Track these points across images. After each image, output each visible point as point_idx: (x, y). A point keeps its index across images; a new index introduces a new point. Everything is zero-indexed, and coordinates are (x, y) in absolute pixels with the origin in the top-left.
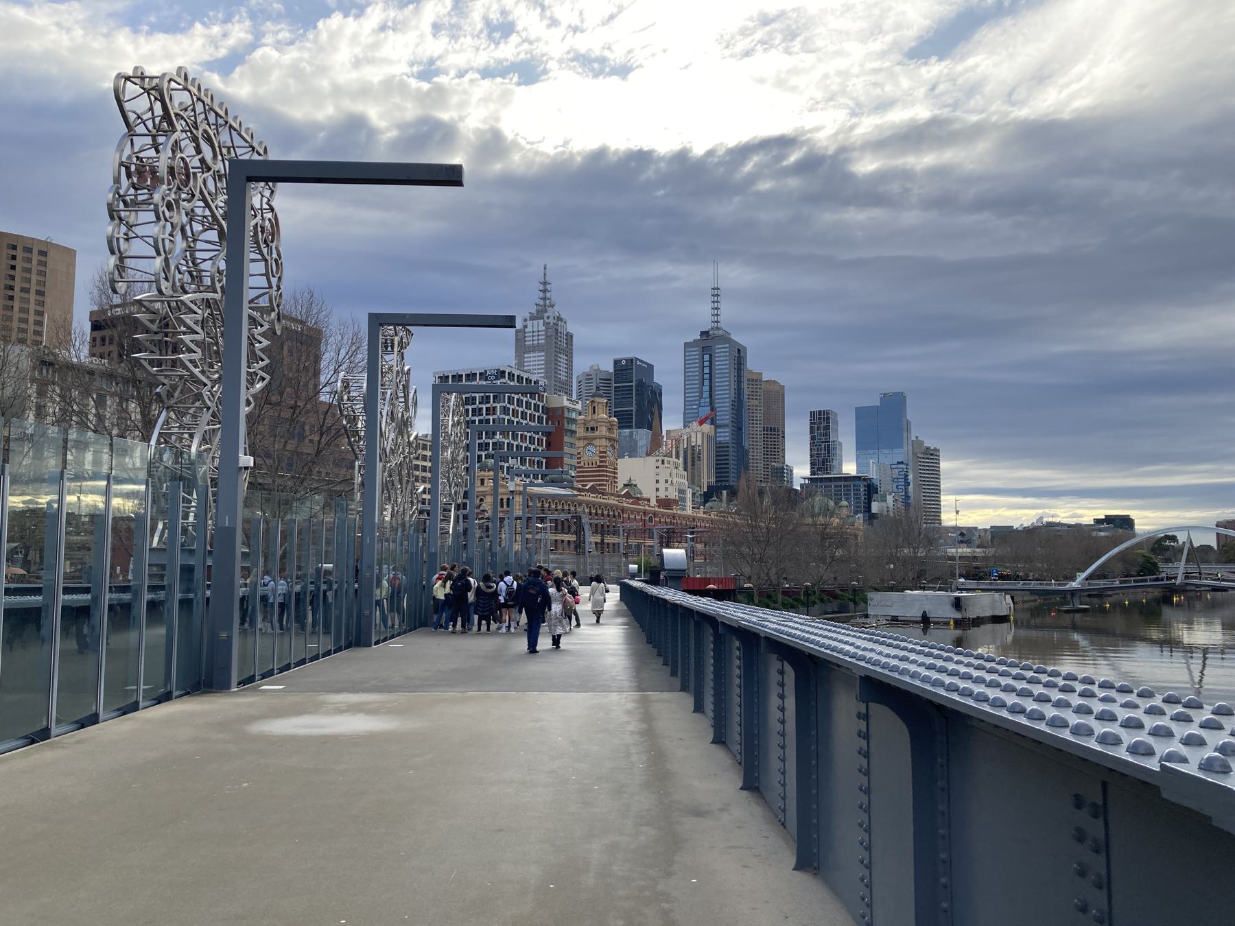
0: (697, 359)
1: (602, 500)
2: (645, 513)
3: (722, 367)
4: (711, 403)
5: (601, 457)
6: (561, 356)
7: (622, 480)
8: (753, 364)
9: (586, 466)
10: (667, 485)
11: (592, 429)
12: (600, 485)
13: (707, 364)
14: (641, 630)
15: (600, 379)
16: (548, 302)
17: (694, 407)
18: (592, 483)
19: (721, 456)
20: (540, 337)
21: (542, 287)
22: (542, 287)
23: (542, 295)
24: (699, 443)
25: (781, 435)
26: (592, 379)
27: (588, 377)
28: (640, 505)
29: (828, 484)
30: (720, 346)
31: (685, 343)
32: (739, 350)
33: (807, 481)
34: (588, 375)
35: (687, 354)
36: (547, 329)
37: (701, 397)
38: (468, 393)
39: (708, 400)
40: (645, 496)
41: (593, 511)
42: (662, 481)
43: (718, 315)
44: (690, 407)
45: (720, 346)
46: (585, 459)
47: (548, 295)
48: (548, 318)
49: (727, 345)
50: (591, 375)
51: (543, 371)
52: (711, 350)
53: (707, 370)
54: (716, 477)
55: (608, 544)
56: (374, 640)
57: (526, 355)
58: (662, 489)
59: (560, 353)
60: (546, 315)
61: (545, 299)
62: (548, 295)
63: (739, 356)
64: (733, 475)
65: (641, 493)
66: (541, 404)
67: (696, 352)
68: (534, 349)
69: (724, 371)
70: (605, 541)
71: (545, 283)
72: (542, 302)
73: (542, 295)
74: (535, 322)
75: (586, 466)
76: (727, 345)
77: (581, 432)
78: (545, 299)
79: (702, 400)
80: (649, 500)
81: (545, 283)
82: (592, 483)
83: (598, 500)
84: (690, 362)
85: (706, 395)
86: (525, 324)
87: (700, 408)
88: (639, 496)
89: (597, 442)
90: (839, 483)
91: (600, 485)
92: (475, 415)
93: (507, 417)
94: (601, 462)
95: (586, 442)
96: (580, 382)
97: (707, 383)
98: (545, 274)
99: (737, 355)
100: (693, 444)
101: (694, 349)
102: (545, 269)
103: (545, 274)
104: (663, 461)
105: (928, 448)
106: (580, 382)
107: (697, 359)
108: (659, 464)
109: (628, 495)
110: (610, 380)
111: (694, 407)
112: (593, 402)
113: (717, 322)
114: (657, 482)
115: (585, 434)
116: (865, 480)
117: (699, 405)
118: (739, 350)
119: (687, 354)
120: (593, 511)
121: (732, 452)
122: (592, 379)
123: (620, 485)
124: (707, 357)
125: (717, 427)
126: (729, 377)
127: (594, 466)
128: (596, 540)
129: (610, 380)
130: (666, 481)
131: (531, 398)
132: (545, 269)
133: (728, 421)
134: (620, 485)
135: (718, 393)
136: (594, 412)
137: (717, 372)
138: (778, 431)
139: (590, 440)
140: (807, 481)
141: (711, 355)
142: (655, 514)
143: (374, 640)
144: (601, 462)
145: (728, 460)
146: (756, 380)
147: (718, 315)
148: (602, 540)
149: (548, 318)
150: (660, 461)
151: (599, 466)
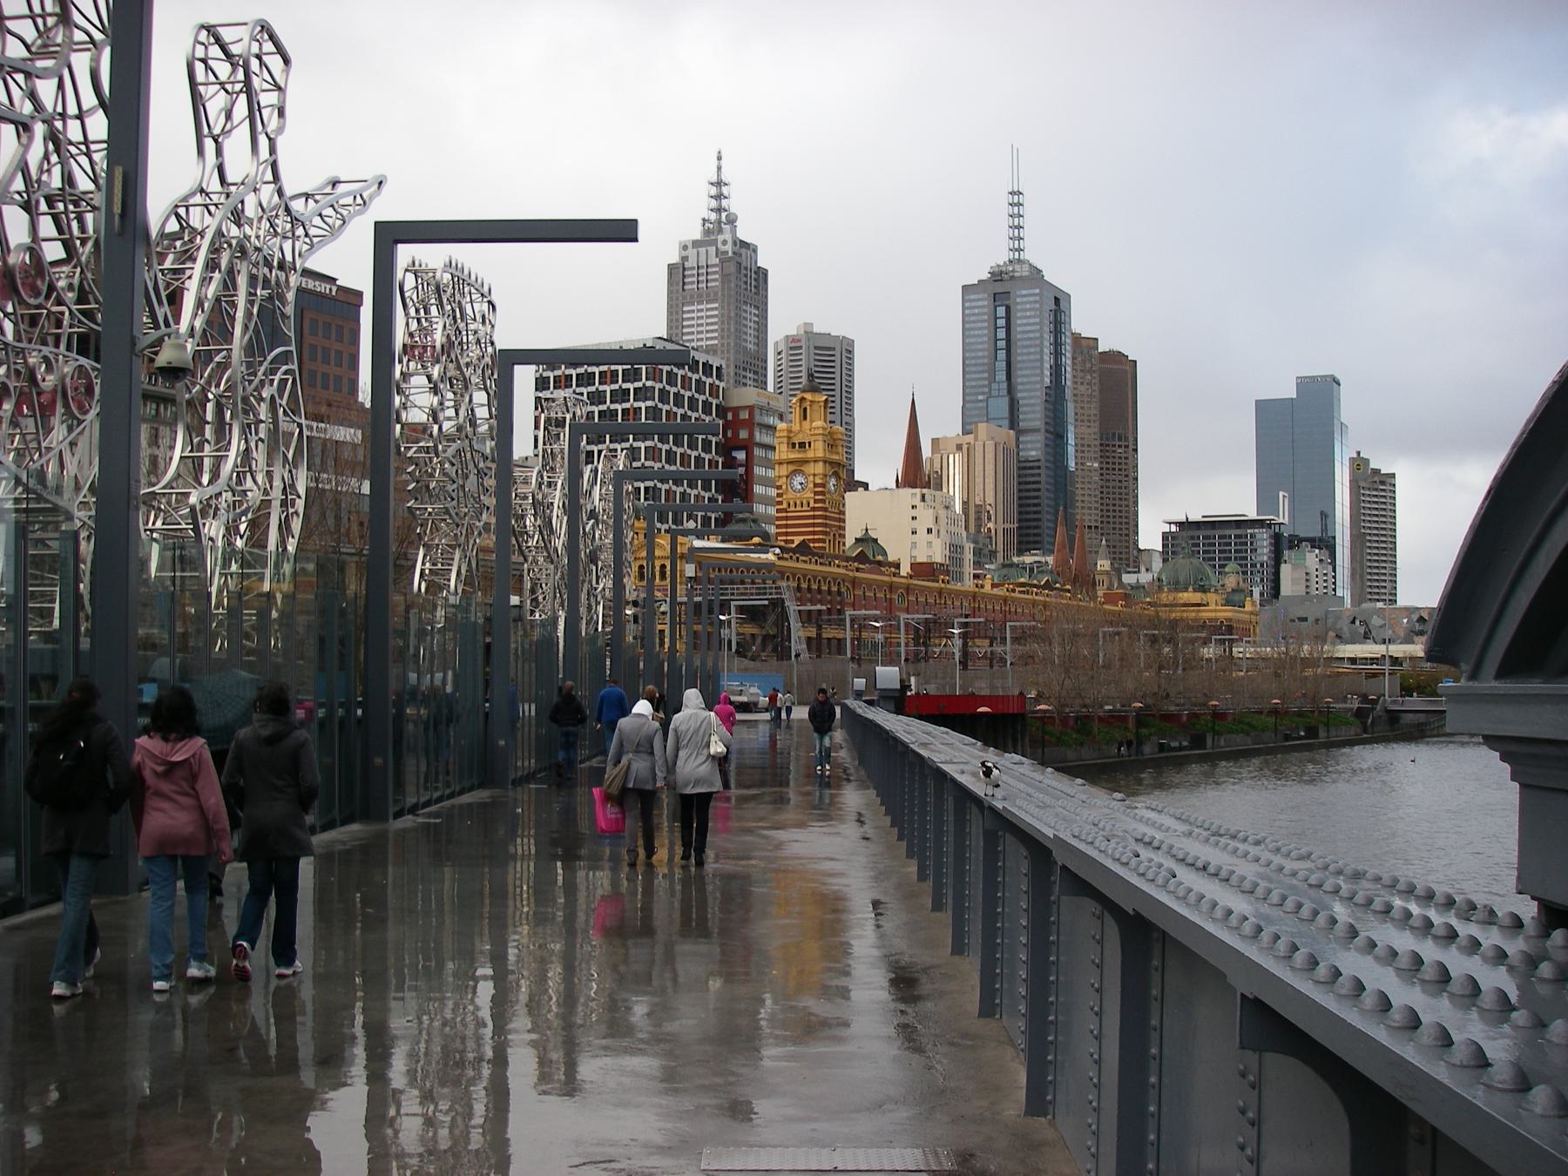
0: (984, 314)
1: (819, 568)
2: (892, 587)
3: (1029, 328)
4: (1011, 390)
5: (816, 493)
6: (748, 308)
7: (852, 532)
8: (1081, 322)
9: (792, 509)
10: (932, 537)
11: (802, 445)
12: (814, 541)
13: (1001, 322)
14: (888, 820)
15: (816, 348)
16: (724, 215)
17: (980, 397)
18: (802, 538)
19: (1027, 483)
20: (709, 277)
21: (714, 191)
22: (714, 191)
23: (714, 204)
24: (990, 499)
25: (1131, 447)
26: (801, 348)
27: (793, 344)
28: (882, 573)
29: (1209, 532)
30: (1024, 292)
31: (964, 287)
32: (1057, 300)
33: (1174, 528)
34: (793, 341)
35: (967, 305)
36: (722, 261)
37: (992, 379)
38: (582, 365)
39: (1005, 385)
40: (890, 559)
41: (804, 586)
42: (922, 531)
43: (1020, 239)
44: (973, 398)
45: (1024, 292)
46: (790, 496)
47: (724, 203)
48: (725, 242)
49: (1037, 291)
50: (799, 341)
51: (716, 320)
52: (1009, 299)
53: (1002, 334)
54: (1020, 521)
55: (829, 639)
56: (392, 810)
57: (685, 309)
58: (922, 545)
59: (745, 303)
60: (720, 238)
61: (719, 210)
62: (724, 203)
63: (1059, 305)
64: (1047, 531)
65: (885, 553)
66: (714, 402)
67: (983, 302)
68: (699, 298)
69: (1032, 335)
70: (824, 635)
71: (719, 184)
72: (713, 216)
73: (714, 204)
74: (702, 250)
75: (792, 509)
76: (1037, 291)
77: (783, 453)
78: (719, 210)
79: (995, 386)
80: (897, 566)
81: (719, 184)
82: (802, 538)
83: (813, 567)
84: (972, 318)
85: (1002, 376)
86: (684, 253)
87: (991, 401)
88: (880, 558)
89: (810, 469)
90: (1227, 532)
91: (814, 541)
92: (605, 383)
93: (658, 386)
94: (816, 501)
95: (792, 468)
96: (779, 353)
97: (1002, 355)
98: (719, 168)
99: (1054, 307)
100: (978, 502)
101: (980, 296)
102: (719, 158)
103: (719, 168)
104: (923, 496)
105: (1376, 472)
106: (779, 353)
107: (984, 314)
108: (917, 501)
109: (862, 558)
110: (834, 349)
111: (980, 397)
112: (803, 399)
113: (1019, 250)
114: (914, 533)
115: (793, 456)
116: (1269, 526)
117: (990, 396)
118: (1057, 300)
119: (967, 305)
120: (804, 586)
121: (1044, 476)
122: (801, 348)
123: (850, 541)
124: (1001, 311)
125: (1020, 432)
126: (1041, 324)
127: (805, 508)
128: (809, 635)
129: (834, 349)
130: (929, 531)
131: (675, 443)
132: (719, 158)
133: (1038, 423)
134: (850, 541)
135: (1020, 377)
136: (805, 418)
137: (1019, 322)
138: (1126, 439)
139: (798, 466)
140: (1174, 528)
141: (1008, 309)
142: (908, 589)
143: (392, 810)
144: (816, 501)
145: (1039, 490)
146: (1086, 346)
147: (1020, 239)
148: (819, 635)
149: (725, 242)
150: (919, 497)
151: (814, 509)
